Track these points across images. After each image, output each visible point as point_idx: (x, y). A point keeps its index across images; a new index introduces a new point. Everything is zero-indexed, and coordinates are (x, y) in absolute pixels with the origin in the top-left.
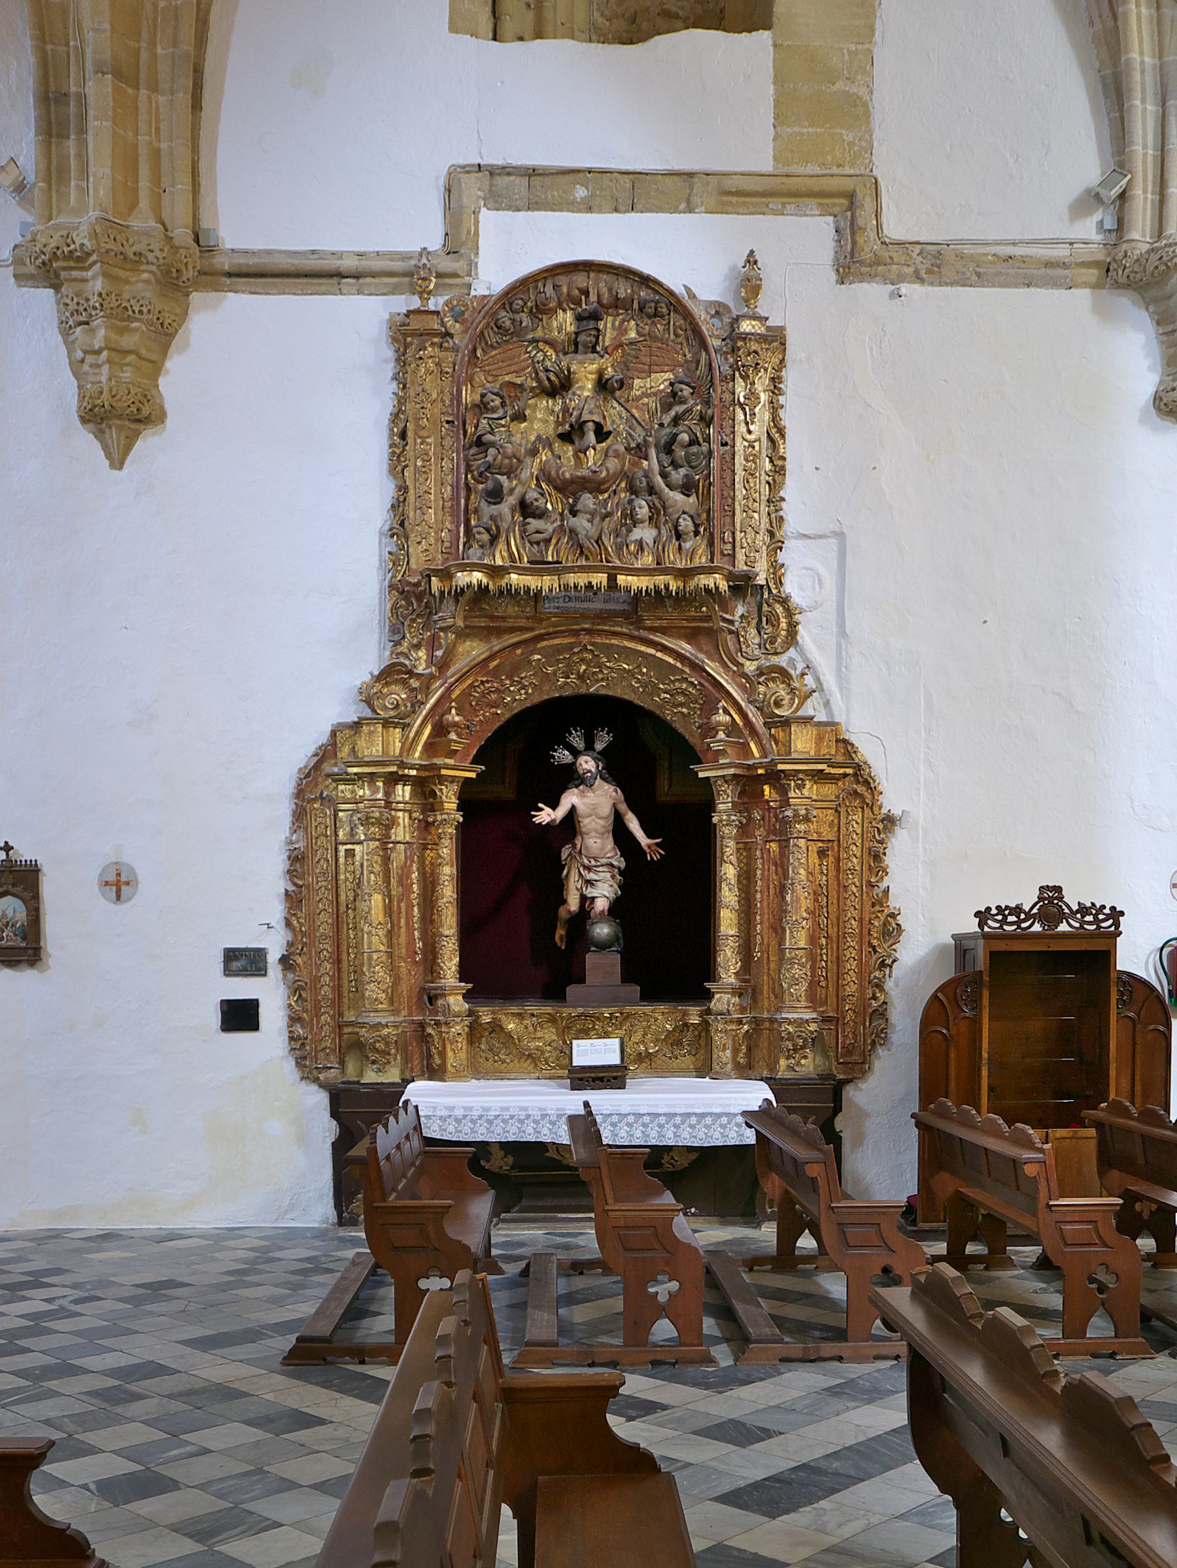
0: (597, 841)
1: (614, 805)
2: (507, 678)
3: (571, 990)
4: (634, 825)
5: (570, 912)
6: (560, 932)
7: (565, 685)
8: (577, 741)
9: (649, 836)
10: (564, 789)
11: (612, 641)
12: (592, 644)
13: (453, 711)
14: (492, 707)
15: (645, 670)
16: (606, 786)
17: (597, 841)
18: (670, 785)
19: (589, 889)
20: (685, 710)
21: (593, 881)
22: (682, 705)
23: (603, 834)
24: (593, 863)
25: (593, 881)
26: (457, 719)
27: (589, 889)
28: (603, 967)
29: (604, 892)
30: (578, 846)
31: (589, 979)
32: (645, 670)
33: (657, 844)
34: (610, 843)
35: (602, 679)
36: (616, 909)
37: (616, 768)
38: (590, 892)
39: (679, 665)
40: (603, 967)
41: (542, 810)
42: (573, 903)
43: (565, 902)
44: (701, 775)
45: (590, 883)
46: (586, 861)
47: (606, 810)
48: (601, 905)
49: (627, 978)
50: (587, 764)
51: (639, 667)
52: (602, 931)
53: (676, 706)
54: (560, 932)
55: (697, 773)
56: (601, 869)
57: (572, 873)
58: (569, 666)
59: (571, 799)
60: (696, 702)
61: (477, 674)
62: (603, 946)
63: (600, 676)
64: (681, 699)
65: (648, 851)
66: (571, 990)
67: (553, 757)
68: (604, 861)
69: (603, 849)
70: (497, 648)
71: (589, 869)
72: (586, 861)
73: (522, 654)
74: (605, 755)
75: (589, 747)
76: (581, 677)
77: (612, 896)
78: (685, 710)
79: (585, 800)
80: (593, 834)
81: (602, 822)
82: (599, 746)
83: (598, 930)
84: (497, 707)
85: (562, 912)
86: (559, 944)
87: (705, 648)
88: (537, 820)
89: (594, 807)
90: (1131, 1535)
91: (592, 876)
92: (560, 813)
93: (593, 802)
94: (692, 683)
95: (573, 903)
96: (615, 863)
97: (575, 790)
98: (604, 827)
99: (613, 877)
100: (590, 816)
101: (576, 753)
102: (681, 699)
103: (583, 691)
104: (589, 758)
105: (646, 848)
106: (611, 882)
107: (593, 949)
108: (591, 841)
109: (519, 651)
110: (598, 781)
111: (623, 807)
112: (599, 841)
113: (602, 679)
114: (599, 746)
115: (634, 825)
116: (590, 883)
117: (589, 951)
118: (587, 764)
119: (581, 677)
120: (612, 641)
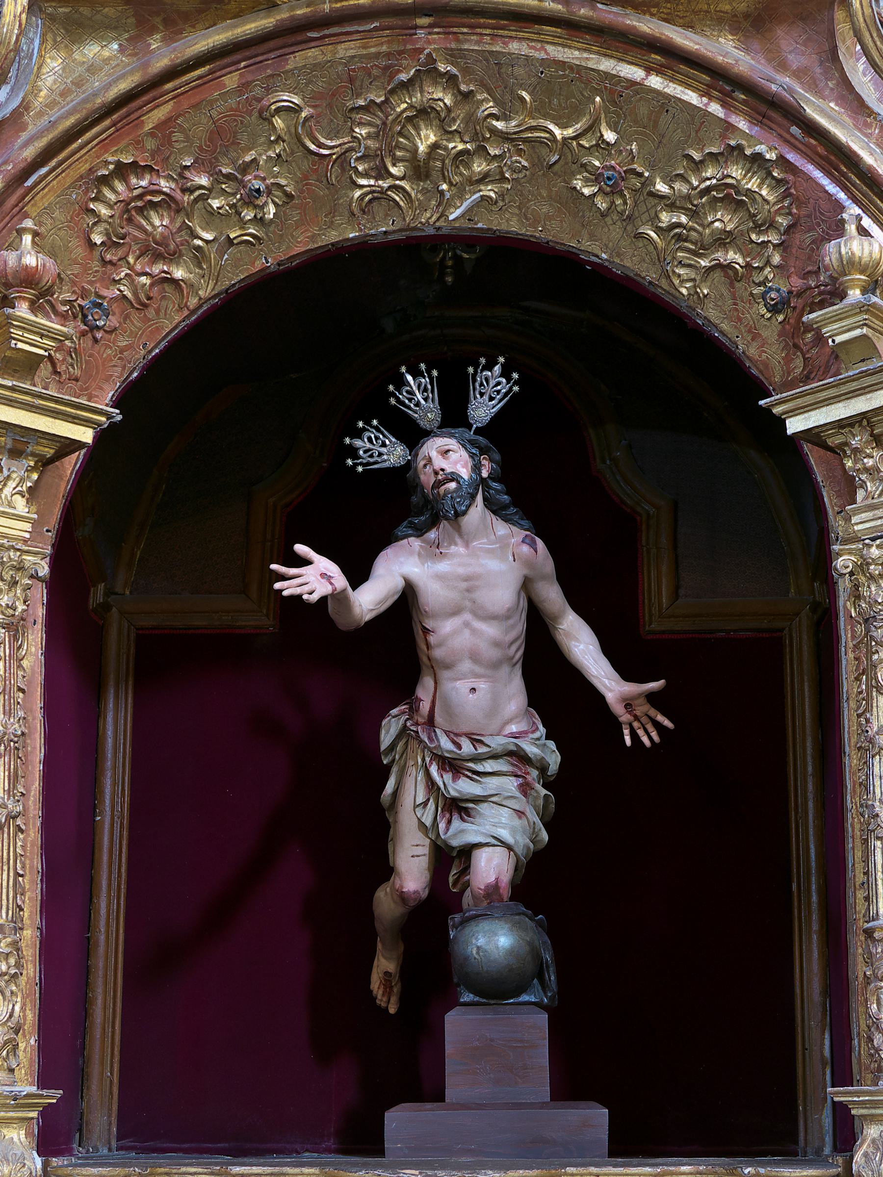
0: (477, 692)
1: (526, 586)
2: (199, 165)
3: (398, 1120)
4: (582, 646)
5: (403, 897)
6: (384, 964)
7: (382, 203)
8: (419, 395)
9: (626, 672)
10: (386, 539)
11: (514, 47)
12: (453, 56)
13: (27, 239)
14: (157, 257)
15: (610, 136)
16: (502, 528)
17: (477, 692)
18: (675, 595)
19: (456, 823)
20: (733, 256)
21: (472, 805)
22: (724, 240)
23: (495, 665)
24: (467, 748)
25: (472, 805)
26: (31, 261)
27: (456, 823)
28: (497, 1050)
29: (501, 831)
30: (425, 707)
31: (456, 1087)
32: (610, 136)
33: (652, 698)
34: (514, 695)
35: (484, 178)
36: (535, 885)
37: (534, 480)
38: (461, 833)
39: (715, 108)
40: (497, 1050)
41: (305, 562)
42: (412, 870)
43: (386, 871)
44: (794, 425)
45: (458, 807)
46: (446, 744)
47: (503, 595)
48: (491, 868)
49: (569, 1086)
50: (449, 458)
51: (592, 128)
52: (495, 941)
53: (702, 248)
54: (384, 964)
55: (781, 423)
56: (489, 766)
57: (409, 783)
58: (382, 132)
59: (399, 566)
60: (772, 225)
61: (105, 145)
62: (497, 989)
63: (479, 167)
64: (722, 220)
65: (625, 718)
66: (398, 1120)
67: (353, 452)
68: (497, 743)
69: (493, 709)
70: (161, 63)
71: (453, 765)
72: (446, 744)
73: (244, 87)
74: (495, 437)
75: (454, 416)
76: (420, 170)
77: (521, 842)
78: (733, 256)
79: (443, 567)
80: (466, 666)
81: (490, 630)
82: (482, 410)
83: (481, 941)
84: (173, 257)
85: (384, 902)
86: (380, 997)
87: (795, 61)
88: (288, 588)
89: (471, 583)
90: (6, 781)
91: (464, 787)
92: (369, 599)
93: (469, 576)
94: (757, 158)
95: (412, 870)
96: (531, 750)
97: (415, 543)
98: (497, 644)
99: (525, 788)
100: (456, 612)
101: (412, 435)
102: (722, 220)
103: (427, 219)
104: (451, 443)
105: (618, 709)
106: (520, 803)
107: (467, 997)
108: (462, 687)
109: (231, 81)
110: (477, 511)
111: (552, 595)
112: (482, 686)
113: (484, 178)
114: (482, 410)
115: (582, 646)
116: (458, 807)
117: (454, 1003)
118: (449, 458)
119: (420, 170)
120: (514, 47)
